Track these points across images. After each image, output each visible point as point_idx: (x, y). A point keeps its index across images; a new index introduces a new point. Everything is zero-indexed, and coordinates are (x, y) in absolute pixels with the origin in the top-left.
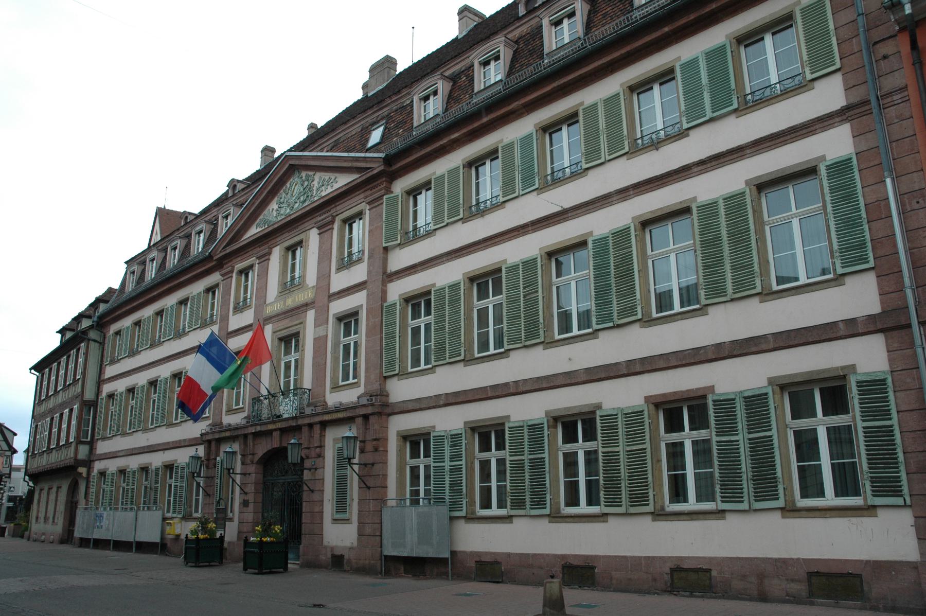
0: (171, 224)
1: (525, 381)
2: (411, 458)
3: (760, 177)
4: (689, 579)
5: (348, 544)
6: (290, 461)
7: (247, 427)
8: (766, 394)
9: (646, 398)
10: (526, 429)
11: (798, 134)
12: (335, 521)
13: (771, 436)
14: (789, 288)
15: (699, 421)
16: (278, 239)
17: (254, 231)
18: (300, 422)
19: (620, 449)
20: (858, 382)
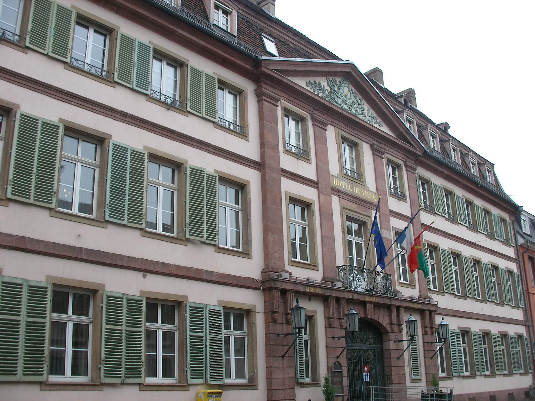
0: (376, 73)
1: (31, 240)
2: (147, 320)
3: (174, 156)
6: (349, 330)
10: (125, 300)
11: (239, 160)
12: (413, 381)
14: (61, 210)
15: (81, 308)
16: (334, 121)
17: (385, 129)
18: (368, 299)
19: (123, 328)
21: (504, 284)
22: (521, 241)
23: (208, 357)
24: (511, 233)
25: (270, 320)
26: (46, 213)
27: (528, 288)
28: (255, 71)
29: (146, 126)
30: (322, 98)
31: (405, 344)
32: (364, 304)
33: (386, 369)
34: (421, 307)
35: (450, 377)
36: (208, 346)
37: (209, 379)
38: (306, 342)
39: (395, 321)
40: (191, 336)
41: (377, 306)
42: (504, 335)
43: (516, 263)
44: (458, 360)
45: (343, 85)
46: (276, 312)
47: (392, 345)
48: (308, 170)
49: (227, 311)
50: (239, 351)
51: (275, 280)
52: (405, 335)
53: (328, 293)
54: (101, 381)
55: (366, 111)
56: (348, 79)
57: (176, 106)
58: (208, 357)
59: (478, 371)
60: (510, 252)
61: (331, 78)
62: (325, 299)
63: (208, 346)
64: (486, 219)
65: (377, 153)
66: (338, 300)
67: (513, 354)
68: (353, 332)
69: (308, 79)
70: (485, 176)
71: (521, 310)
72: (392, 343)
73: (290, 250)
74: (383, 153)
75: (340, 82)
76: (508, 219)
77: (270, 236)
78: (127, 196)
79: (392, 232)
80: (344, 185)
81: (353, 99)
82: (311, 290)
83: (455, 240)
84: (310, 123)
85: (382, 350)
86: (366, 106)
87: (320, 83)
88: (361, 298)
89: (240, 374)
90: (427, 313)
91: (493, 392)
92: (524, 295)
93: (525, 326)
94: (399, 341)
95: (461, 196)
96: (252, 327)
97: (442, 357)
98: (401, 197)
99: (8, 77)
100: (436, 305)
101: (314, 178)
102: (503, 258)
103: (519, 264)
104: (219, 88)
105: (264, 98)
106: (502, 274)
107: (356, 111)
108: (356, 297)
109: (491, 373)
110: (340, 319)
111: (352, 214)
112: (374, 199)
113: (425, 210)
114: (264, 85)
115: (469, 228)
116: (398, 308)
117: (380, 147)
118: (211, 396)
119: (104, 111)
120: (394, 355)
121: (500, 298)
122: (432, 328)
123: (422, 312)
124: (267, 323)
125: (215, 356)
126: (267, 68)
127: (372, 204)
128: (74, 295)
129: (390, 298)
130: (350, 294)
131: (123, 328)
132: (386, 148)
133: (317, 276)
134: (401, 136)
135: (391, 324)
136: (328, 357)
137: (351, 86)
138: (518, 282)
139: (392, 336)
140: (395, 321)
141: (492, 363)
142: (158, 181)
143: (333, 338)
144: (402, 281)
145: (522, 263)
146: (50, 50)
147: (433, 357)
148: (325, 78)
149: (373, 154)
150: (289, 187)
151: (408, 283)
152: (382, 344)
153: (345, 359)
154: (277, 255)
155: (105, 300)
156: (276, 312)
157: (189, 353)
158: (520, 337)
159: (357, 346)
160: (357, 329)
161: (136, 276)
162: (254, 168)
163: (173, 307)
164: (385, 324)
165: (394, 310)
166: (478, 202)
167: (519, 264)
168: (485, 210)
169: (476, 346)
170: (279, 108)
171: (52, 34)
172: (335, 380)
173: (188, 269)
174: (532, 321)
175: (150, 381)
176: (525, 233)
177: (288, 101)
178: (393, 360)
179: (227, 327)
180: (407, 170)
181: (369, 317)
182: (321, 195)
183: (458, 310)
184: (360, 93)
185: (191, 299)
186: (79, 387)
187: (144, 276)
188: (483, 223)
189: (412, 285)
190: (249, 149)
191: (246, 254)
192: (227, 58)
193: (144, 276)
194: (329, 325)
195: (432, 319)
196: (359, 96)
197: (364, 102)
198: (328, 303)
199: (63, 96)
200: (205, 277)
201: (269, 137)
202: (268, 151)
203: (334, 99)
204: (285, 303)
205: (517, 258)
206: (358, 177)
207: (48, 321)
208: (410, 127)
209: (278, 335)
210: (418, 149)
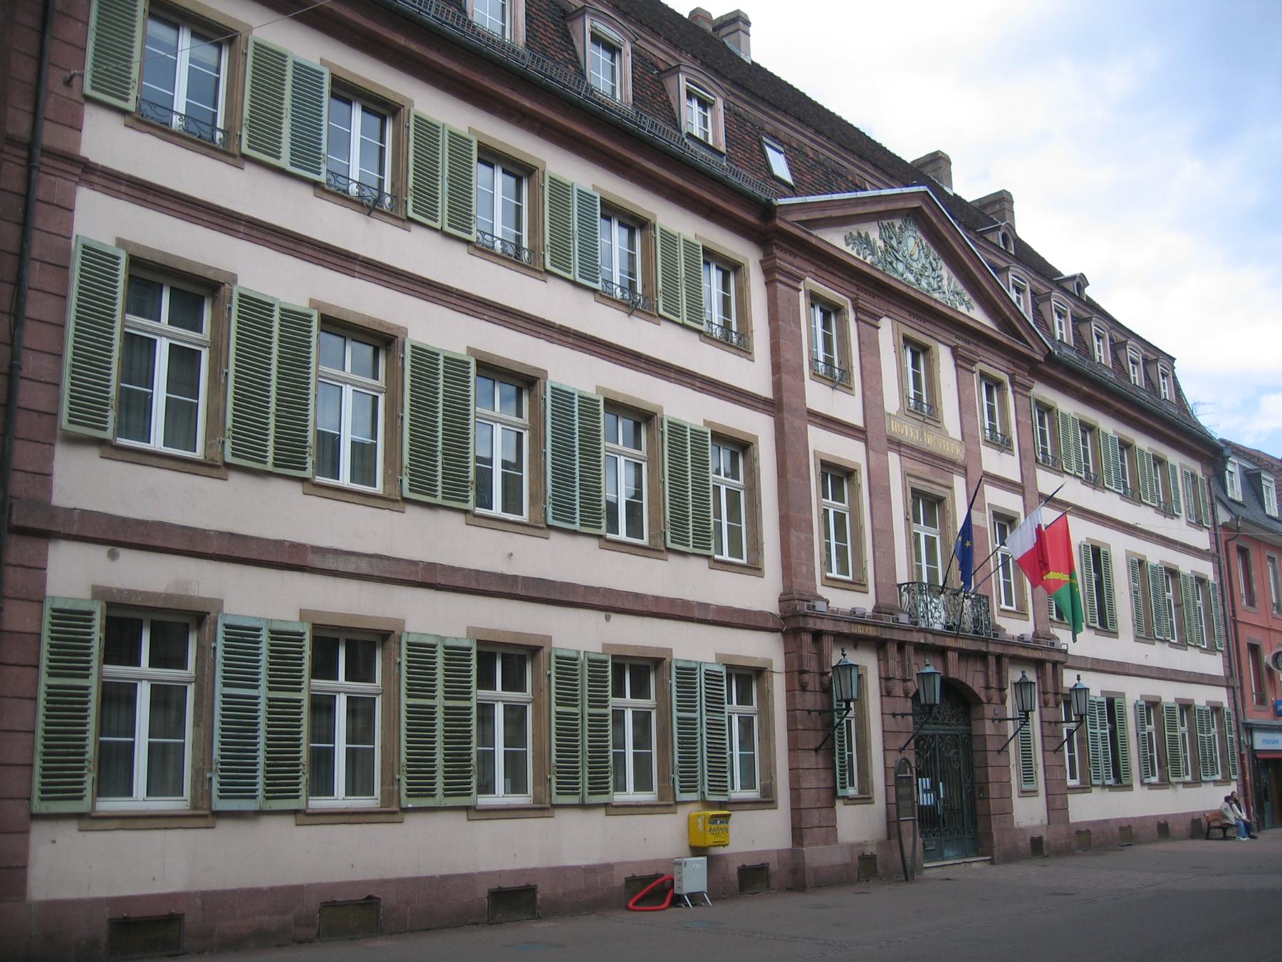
2: (480, 686)
4: (514, 900)
5: (1037, 822)
6: (923, 701)
7: (910, 630)
8: (91, 613)
9: (469, 628)
12: (1024, 793)
13: (86, 688)
16: (894, 309)
17: (977, 315)
18: (949, 642)
19: (587, 710)
20: (54, 610)
21: (1188, 606)
22: (1223, 517)
23: (705, 753)
24: (1204, 501)
25: (797, 686)
26: (297, 488)
27: (1234, 612)
28: (763, 225)
29: (598, 350)
30: (871, 266)
31: (1010, 728)
32: (941, 652)
33: (977, 771)
34: (1038, 655)
35: (1085, 787)
36: (705, 735)
37: (706, 791)
38: (1184, 735)
39: (994, 683)
40: (557, 713)
41: (964, 655)
42: (1186, 706)
43: (1213, 561)
44: (1101, 754)
45: (907, 234)
46: (805, 672)
47: (989, 728)
48: (848, 408)
49: (485, 649)
50: (746, 742)
51: (805, 615)
52: (1010, 708)
53: (887, 635)
54: (214, 809)
55: (945, 282)
56: (915, 219)
57: (635, 304)
58: (705, 753)
59: (1097, 778)
60: (1202, 540)
61: (885, 223)
62: (879, 645)
63: (705, 735)
64: (1122, 459)
65: (962, 362)
66: (901, 645)
67: (1203, 744)
68: (931, 706)
69: (847, 230)
70: (1049, 323)
71: (1220, 655)
72: (988, 723)
73: (824, 559)
74: (973, 363)
75: (900, 228)
76: (1199, 473)
77: (794, 536)
78: (577, 480)
79: (988, 514)
80: (908, 431)
81: (923, 260)
82: (859, 630)
83: (1098, 523)
84: (851, 316)
85: (970, 735)
86: (945, 271)
87: (867, 235)
88: (939, 641)
89: (748, 783)
90: (1049, 667)
91: (1127, 819)
92: (1226, 625)
93: (1227, 687)
94: (1000, 720)
95: (1111, 433)
96: (765, 698)
97: (1071, 750)
98: (1003, 445)
99: (386, 278)
100: (1066, 652)
101: (859, 422)
102: (1188, 553)
103: (1219, 563)
104: (480, 160)
105: (778, 276)
106: (1186, 585)
107: (929, 284)
108: (930, 639)
109: (1161, 779)
110: (905, 680)
111: (921, 485)
112: (957, 453)
113: (1045, 465)
114: (777, 253)
115: (1124, 496)
116: (999, 658)
117: (970, 352)
118: (715, 822)
119: (534, 328)
120: (992, 745)
121: (1180, 633)
122: (1056, 694)
123: (1039, 664)
124: (790, 691)
125: (598, 752)
126: (785, 221)
127: (953, 463)
128: (631, 667)
129: (986, 641)
130: (922, 635)
131: (263, 693)
132: (979, 351)
133: (865, 603)
134: (1006, 325)
135: (988, 688)
136: (885, 750)
137: (919, 234)
138: (1215, 600)
139: (989, 710)
140: (994, 683)
141: (1163, 759)
142: (342, 373)
143: (894, 715)
144: (1003, 606)
145: (1224, 562)
146: (446, 221)
147: (1059, 749)
148: (875, 224)
149: (957, 366)
150: (822, 443)
151: (1014, 608)
152: (969, 725)
153: (913, 753)
154: (804, 569)
155: (553, 664)
156: (805, 672)
157: (676, 749)
158: (1216, 709)
159: (930, 729)
160: (938, 701)
161: (592, 619)
162: (764, 411)
163: (750, 676)
164: (976, 689)
165: (992, 660)
166: (1143, 443)
167: (1219, 563)
168: (1121, 442)
169: (1202, 731)
170: (802, 294)
171: (446, 190)
172: (902, 791)
173: (672, 601)
174: (1241, 678)
175: (319, 803)
176: (1232, 501)
177: (817, 277)
178: (990, 755)
179: (619, 692)
180: (1014, 392)
181: (951, 675)
182: (871, 453)
183: (1122, 662)
184: (936, 247)
185: (409, 627)
186: (141, 823)
187: (113, 556)
188: (1151, 486)
189: (1021, 613)
190: (753, 375)
191: (754, 568)
192: (717, 206)
193: (113, 556)
194: (887, 693)
195: (1057, 678)
196: (934, 253)
197: (941, 263)
198: (886, 651)
199: (471, 306)
200: (696, 614)
201: (787, 355)
202: (787, 379)
203: (891, 263)
204: (821, 657)
205: (1214, 550)
206: (924, 408)
207: (93, 683)
208: (1018, 299)
209: (809, 712)
210: (1036, 349)
